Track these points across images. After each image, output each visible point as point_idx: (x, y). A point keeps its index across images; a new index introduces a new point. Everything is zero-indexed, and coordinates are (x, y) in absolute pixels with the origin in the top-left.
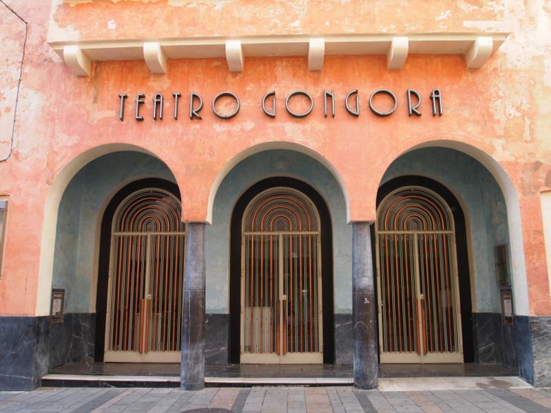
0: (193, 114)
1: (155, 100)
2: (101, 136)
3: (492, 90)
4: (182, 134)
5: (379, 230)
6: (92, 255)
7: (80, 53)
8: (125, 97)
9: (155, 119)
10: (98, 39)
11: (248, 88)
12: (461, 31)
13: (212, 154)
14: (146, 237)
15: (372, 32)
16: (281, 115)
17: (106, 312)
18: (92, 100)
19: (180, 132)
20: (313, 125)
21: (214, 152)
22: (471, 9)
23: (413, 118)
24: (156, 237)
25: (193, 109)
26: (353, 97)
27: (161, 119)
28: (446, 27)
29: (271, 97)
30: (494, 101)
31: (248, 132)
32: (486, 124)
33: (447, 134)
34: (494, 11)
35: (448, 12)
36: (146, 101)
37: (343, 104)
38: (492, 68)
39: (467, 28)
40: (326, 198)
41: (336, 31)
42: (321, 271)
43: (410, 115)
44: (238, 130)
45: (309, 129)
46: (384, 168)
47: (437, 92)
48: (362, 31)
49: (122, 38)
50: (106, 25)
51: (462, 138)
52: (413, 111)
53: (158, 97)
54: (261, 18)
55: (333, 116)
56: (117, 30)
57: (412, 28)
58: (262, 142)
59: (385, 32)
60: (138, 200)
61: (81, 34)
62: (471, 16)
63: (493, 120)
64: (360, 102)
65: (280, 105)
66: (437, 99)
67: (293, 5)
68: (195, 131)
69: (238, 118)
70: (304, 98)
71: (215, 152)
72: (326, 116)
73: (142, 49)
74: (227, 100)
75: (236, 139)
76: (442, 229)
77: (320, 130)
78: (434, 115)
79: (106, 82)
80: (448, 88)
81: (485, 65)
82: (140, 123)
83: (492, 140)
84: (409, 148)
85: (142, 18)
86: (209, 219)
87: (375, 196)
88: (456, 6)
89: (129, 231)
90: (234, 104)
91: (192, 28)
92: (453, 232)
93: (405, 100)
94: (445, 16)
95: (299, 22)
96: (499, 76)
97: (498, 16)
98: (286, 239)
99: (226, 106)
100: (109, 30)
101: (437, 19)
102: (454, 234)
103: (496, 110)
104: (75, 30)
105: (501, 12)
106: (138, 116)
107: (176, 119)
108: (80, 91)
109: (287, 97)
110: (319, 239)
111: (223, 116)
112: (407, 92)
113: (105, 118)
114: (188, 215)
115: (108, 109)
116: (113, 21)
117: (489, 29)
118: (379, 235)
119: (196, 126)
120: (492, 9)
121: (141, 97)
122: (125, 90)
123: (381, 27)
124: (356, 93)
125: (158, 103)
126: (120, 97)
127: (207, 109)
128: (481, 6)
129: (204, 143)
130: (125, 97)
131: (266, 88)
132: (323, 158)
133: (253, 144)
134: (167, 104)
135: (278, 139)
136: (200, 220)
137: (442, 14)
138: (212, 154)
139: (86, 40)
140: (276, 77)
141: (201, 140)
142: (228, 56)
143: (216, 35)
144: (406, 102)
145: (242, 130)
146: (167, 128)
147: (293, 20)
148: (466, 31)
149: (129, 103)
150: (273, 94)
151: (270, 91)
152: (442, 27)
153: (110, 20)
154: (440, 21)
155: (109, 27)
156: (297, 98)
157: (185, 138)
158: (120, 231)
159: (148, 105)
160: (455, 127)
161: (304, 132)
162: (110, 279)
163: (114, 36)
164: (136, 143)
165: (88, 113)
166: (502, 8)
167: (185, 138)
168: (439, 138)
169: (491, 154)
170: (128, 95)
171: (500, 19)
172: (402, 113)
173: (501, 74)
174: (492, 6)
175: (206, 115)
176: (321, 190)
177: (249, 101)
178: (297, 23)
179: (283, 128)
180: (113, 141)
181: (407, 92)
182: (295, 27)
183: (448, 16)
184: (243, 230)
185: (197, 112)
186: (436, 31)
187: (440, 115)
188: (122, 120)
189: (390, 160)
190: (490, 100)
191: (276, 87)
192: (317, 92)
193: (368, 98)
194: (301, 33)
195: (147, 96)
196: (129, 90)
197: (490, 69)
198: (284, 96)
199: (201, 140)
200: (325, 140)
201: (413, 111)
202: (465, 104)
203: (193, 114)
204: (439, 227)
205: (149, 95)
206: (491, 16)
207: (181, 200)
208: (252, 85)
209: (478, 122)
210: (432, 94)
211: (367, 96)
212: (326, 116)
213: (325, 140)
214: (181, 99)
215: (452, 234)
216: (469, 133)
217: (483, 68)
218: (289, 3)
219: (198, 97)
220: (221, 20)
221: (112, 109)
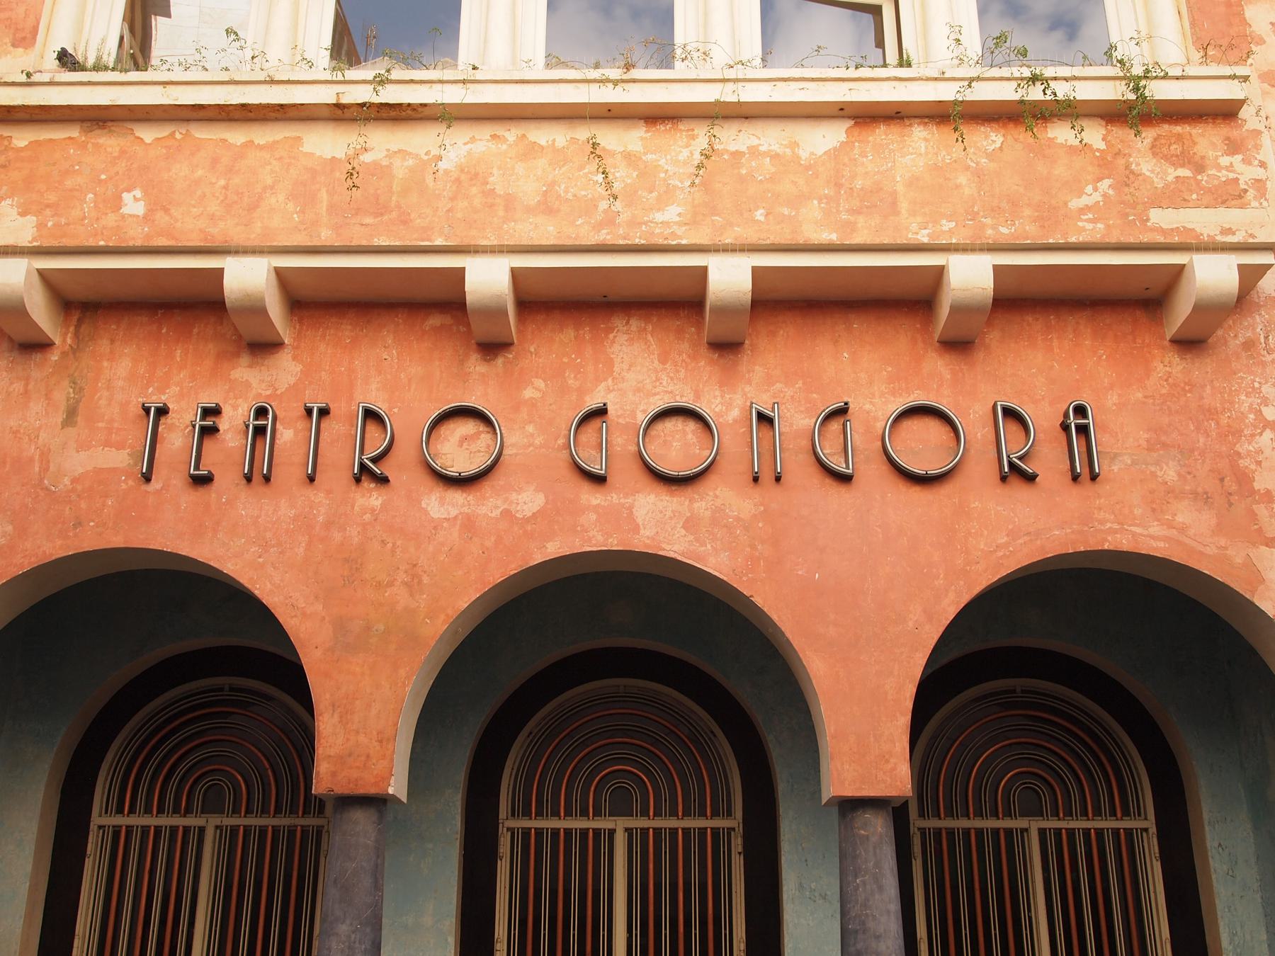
0: (363, 467)
1: (252, 423)
2: (79, 524)
3: (1245, 402)
4: (328, 525)
5: (922, 815)
6: (24, 889)
7: (36, 279)
8: (162, 412)
9: (248, 479)
10: (91, 242)
11: (528, 393)
12: (1146, 238)
13: (413, 585)
14: (202, 830)
15: (886, 240)
16: (625, 474)
17: (72, 947)
18: (60, 417)
19: (321, 519)
20: (719, 502)
21: (420, 582)
22: (1170, 178)
23: (1015, 482)
24: (234, 830)
25: (362, 452)
26: (835, 426)
27: (267, 479)
28: (1100, 226)
29: (595, 423)
30: (1253, 435)
31: (527, 520)
32: (1231, 504)
33: (1115, 532)
34: (1237, 180)
35: (1105, 185)
36: (223, 424)
37: (805, 443)
38: (1241, 339)
39: (1163, 231)
40: (759, 718)
41: (785, 238)
42: (743, 946)
43: (1004, 479)
44: (497, 513)
45: (708, 513)
46: (932, 635)
47: (1080, 411)
48: (858, 239)
49: (162, 242)
50: (117, 204)
51: (1161, 544)
52: (1011, 464)
53: (261, 412)
54: (570, 196)
55: (778, 479)
56: (147, 218)
57: (1004, 230)
58: (567, 551)
59: (925, 240)
60: (193, 709)
61: (40, 226)
62: (1174, 197)
63: (1253, 492)
64: (857, 436)
65: (622, 443)
66: (1083, 430)
67: (662, 162)
68: (367, 517)
69: (498, 479)
70: (691, 426)
71: (426, 580)
72: (756, 479)
73: (219, 273)
74: (467, 427)
75: (489, 543)
76: (1113, 814)
77: (738, 519)
78: (1075, 478)
79: (105, 364)
80: (1112, 399)
81: (1220, 332)
82: (202, 491)
83: (1253, 553)
84: (1003, 573)
85: (226, 187)
86: (397, 787)
87: (904, 720)
88: (1127, 167)
89: (148, 811)
90: (485, 438)
91: (368, 220)
92: (1150, 824)
93: (989, 430)
94: (1097, 197)
95: (680, 210)
96: (1263, 364)
97: (1251, 194)
98: (637, 838)
99: (461, 443)
100: (123, 216)
101: (1075, 204)
102: (1153, 830)
103: (1259, 463)
104: (23, 214)
105: (1260, 185)
106: (197, 467)
107: (311, 479)
108: (26, 392)
109: (642, 418)
110: (737, 843)
111: (453, 471)
112: (994, 407)
113: (98, 471)
114: (334, 774)
115: (107, 444)
116: (138, 193)
117: (1230, 231)
118: (923, 831)
119: (371, 498)
120: (1231, 176)
121: (212, 412)
122: (162, 391)
123: (914, 227)
124: (842, 411)
125: (260, 431)
126: (147, 411)
127: (405, 452)
128: (1200, 168)
129: (393, 551)
130: (162, 412)
131: (582, 392)
132: (747, 601)
133: (538, 558)
134: (286, 435)
135: (614, 544)
136: (373, 791)
137: (1089, 189)
138: (413, 585)
139: (54, 243)
140: (610, 363)
141: (383, 542)
142: (469, 298)
143: (439, 242)
144: (992, 437)
145: (507, 514)
146: (283, 503)
147: (661, 204)
148: (1160, 239)
149: (171, 428)
150: (601, 412)
151: (593, 402)
152: (1089, 226)
153: (129, 191)
154: (1082, 211)
155: (125, 210)
156: (672, 426)
157: (337, 536)
158: (120, 810)
159: (229, 436)
160: (1138, 512)
161: (691, 524)
162: (88, 863)
163: (136, 237)
164: (185, 549)
165: (45, 456)
166: (1259, 173)
167: (337, 536)
168: (1093, 544)
169: (1253, 593)
170: (171, 406)
171: (1255, 204)
172: (981, 468)
173: (1269, 358)
174: (1230, 168)
175: (400, 469)
176: (743, 692)
177: (530, 429)
178: (672, 213)
179: (630, 509)
180: (117, 541)
181: (994, 407)
182: (666, 224)
183: (1105, 195)
184: (502, 815)
185: (375, 460)
186: (1073, 239)
187: (1094, 477)
188: (147, 478)
189: (949, 609)
190: (1238, 433)
191: (609, 390)
192: (729, 405)
193: (880, 425)
194: (684, 242)
195: (227, 410)
196: (174, 390)
197: (1235, 343)
198: (635, 417)
199: (383, 542)
200: (753, 547)
201: (1011, 464)
202: (1165, 446)
203: (363, 467)
204: (1105, 806)
205: (235, 407)
206: (1230, 195)
207: (313, 716)
208: (540, 383)
209: (1204, 499)
210: (1066, 415)
211: (876, 419)
212: (756, 479)
213: (753, 547)
214: (325, 424)
215: (1146, 830)
216: (1183, 529)
217: (1210, 341)
218: (650, 157)
219: (427, 152)
220: (452, 199)
221: (120, 446)
